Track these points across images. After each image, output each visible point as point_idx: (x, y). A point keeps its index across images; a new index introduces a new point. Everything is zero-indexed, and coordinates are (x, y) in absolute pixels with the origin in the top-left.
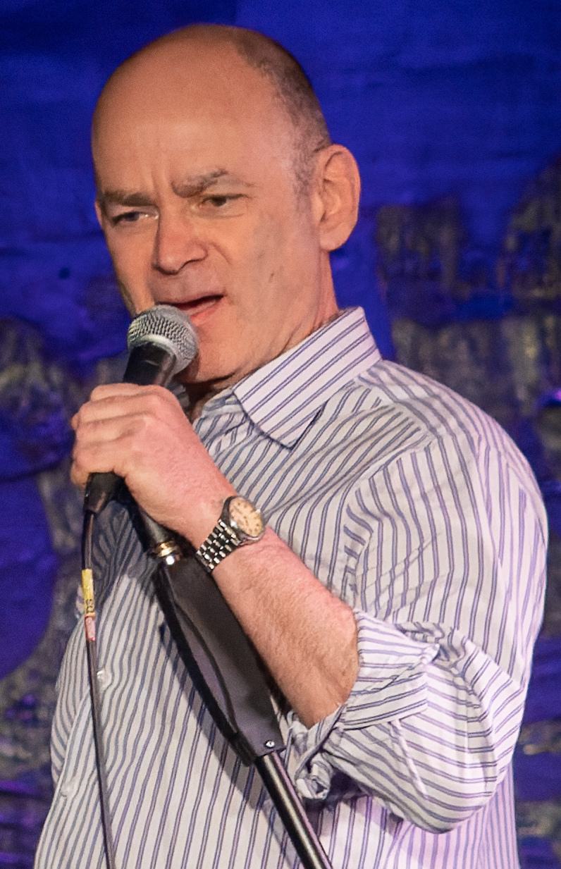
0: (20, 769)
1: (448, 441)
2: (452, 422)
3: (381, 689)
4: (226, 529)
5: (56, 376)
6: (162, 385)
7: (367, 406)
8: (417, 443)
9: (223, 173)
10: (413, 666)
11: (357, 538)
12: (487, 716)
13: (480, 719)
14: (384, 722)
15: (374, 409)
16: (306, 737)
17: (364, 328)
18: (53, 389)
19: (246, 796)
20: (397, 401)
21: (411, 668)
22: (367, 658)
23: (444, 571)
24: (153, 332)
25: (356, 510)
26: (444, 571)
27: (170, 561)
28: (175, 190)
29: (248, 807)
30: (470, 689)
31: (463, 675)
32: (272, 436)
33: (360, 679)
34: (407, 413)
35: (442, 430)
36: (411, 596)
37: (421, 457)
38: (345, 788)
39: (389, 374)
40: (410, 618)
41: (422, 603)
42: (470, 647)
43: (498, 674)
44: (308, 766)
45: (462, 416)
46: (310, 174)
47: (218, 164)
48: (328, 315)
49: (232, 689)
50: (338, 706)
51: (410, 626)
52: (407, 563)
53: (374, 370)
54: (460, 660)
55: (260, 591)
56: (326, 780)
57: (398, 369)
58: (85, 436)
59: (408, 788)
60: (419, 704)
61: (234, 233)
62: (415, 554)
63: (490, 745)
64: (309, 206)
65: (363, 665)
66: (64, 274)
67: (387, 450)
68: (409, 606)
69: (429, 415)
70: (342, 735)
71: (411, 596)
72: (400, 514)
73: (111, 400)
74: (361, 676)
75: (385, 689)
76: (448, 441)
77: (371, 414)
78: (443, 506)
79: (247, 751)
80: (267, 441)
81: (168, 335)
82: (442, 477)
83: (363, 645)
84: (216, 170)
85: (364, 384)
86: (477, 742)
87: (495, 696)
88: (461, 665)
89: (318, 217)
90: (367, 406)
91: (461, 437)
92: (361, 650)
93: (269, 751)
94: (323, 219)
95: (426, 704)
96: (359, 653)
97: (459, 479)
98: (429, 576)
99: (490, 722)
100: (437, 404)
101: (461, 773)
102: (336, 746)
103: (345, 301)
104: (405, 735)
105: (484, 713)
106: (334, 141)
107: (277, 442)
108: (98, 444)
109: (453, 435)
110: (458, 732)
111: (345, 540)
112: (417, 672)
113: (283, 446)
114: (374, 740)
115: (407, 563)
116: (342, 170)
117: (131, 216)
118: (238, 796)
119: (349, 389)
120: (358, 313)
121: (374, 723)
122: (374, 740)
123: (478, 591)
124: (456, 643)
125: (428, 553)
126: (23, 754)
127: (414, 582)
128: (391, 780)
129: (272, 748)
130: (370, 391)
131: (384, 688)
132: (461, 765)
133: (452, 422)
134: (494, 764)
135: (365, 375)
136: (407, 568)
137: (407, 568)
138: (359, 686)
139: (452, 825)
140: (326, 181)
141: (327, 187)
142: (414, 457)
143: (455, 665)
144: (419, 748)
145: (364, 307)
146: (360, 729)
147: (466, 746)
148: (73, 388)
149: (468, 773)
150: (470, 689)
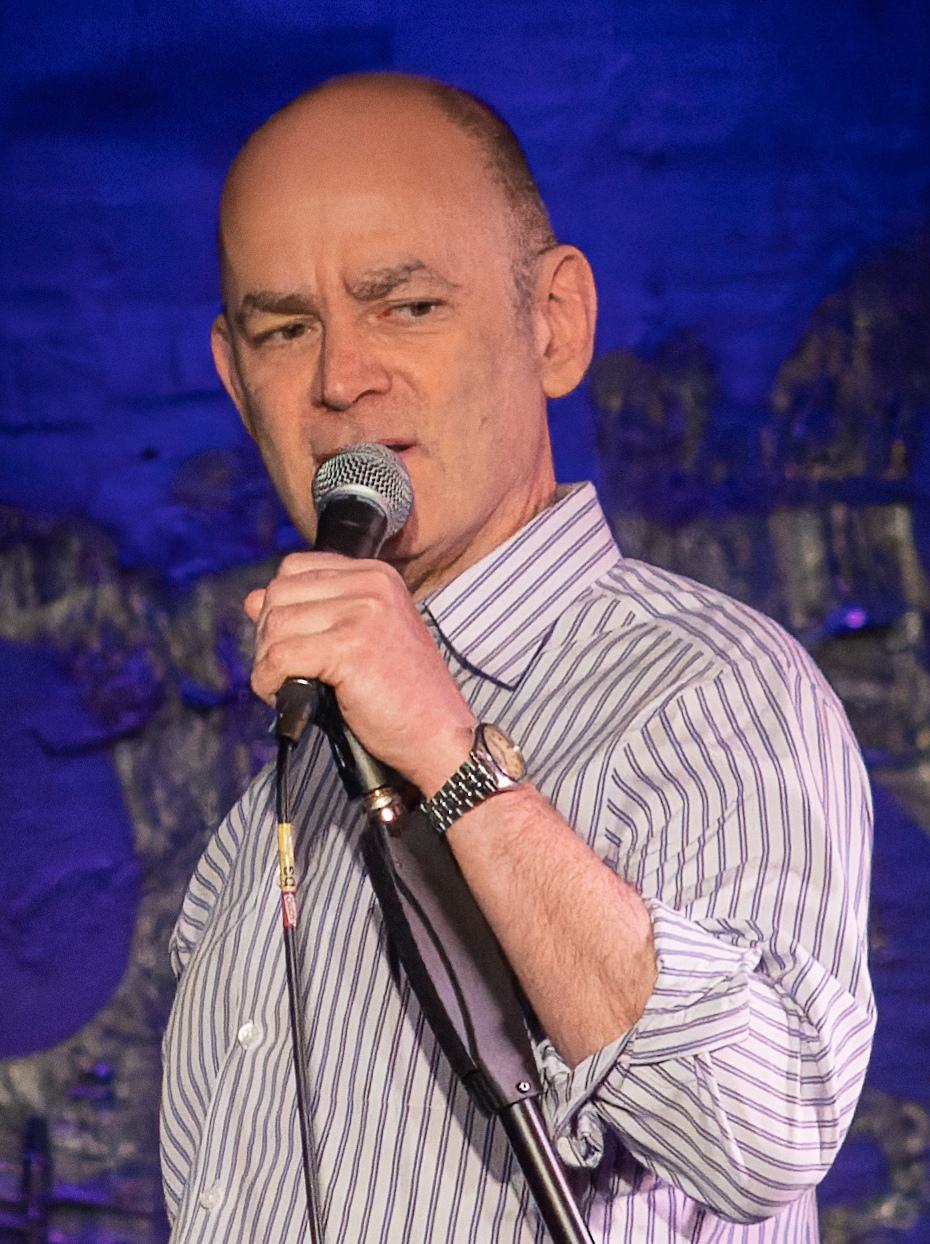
0: (88, 1169)
1: (745, 667)
2: (748, 643)
3: (689, 1007)
4: (480, 766)
5: (138, 603)
6: (371, 556)
7: (615, 624)
8: (701, 673)
9: (421, 266)
10: (731, 976)
11: (625, 819)
12: (826, 1054)
13: (815, 1058)
14: (688, 1055)
15: (627, 628)
16: (571, 1078)
17: (596, 514)
18: (133, 619)
19: (486, 1160)
20: (658, 616)
21: (729, 979)
22: (669, 961)
23: (755, 851)
24: (357, 482)
25: (626, 773)
26: (755, 851)
27: (387, 816)
28: (348, 288)
29: (490, 1178)
30: (801, 1013)
31: (793, 997)
32: (484, 670)
33: (656, 991)
34: (678, 632)
35: (734, 653)
36: (708, 886)
37: (711, 693)
38: (620, 1163)
39: (639, 576)
40: (710, 913)
41: (725, 894)
42: (804, 955)
43: (838, 995)
44: (574, 1121)
45: (759, 633)
46: (532, 283)
47: (400, 274)
48: (546, 494)
49: (480, 1019)
50: (622, 1033)
51: (714, 925)
52: (702, 843)
53: (617, 572)
54: (786, 973)
55: (519, 861)
56: (598, 1140)
57: (652, 572)
58: (283, 627)
59: (718, 1157)
60: (740, 1030)
61: (426, 356)
62: (714, 826)
63: (830, 1096)
64: (530, 328)
65: (664, 971)
66: (149, 455)
67: (660, 687)
68: (707, 899)
69: (711, 632)
70: (627, 1074)
71: (708, 886)
72: (693, 774)
73: (316, 575)
74: (657, 986)
75: (694, 1007)
76: (745, 667)
77: (621, 637)
78: (752, 757)
79: (490, 1094)
80: (478, 678)
81: (378, 486)
82: (744, 718)
83: (660, 943)
84: (407, 262)
85: (609, 593)
86: (810, 1091)
87: (836, 1025)
88: (789, 980)
89: (542, 348)
90: (615, 624)
91: (764, 662)
92: (659, 950)
93: (522, 1096)
94: (549, 352)
95: (748, 1032)
96: (657, 954)
97: (769, 720)
98: (733, 860)
99: (832, 1062)
100: (719, 618)
101: (791, 1133)
102: (616, 1092)
103: (568, 472)
104: (717, 1077)
105: (825, 1049)
106: (563, 240)
107: (493, 680)
108: (299, 639)
109: (752, 660)
110: (790, 1076)
111: (608, 820)
112: (739, 983)
113: (500, 685)
114: (670, 1079)
115: (702, 843)
116: (572, 283)
117: (293, 331)
118: (475, 1162)
119: (586, 599)
120: (587, 492)
121: (674, 1056)
122: (670, 1079)
123: (806, 878)
124: (782, 949)
125: (732, 827)
126: (94, 1147)
127: (712, 869)
128: (690, 1142)
129: (525, 1092)
130: (619, 602)
131: (693, 1005)
132: (791, 1122)
133: (748, 643)
134: (834, 1123)
135: (606, 580)
136: (701, 850)
137: (701, 850)
138: (655, 1002)
139: (766, 1210)
140: (551, 297)
141: (554, 304)
142: (699, 692)
143: (779, 981)
144: (736, 1096)
145: (595, 483)
146: (650, 1065)
147: (798, 1095)
148: (162, 621)
149: (800, 1135)
150: (801, 1013)
